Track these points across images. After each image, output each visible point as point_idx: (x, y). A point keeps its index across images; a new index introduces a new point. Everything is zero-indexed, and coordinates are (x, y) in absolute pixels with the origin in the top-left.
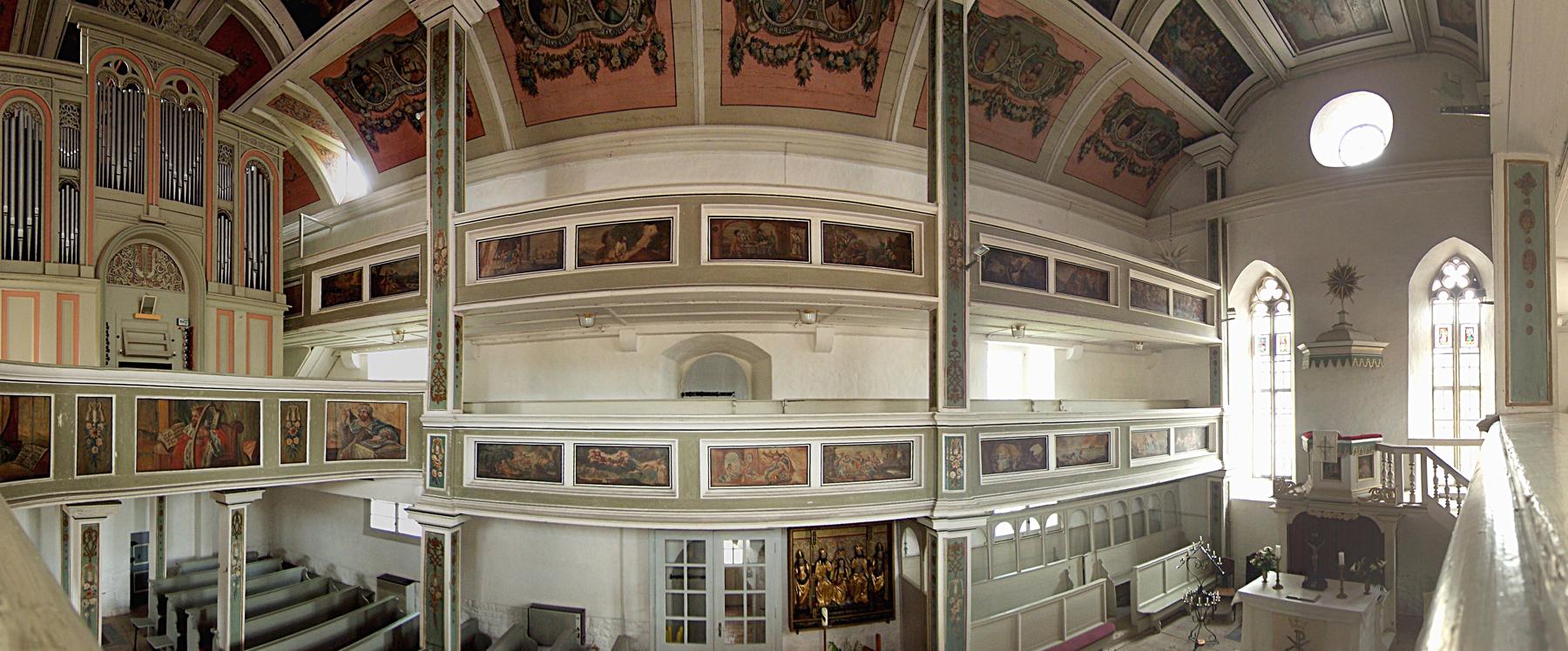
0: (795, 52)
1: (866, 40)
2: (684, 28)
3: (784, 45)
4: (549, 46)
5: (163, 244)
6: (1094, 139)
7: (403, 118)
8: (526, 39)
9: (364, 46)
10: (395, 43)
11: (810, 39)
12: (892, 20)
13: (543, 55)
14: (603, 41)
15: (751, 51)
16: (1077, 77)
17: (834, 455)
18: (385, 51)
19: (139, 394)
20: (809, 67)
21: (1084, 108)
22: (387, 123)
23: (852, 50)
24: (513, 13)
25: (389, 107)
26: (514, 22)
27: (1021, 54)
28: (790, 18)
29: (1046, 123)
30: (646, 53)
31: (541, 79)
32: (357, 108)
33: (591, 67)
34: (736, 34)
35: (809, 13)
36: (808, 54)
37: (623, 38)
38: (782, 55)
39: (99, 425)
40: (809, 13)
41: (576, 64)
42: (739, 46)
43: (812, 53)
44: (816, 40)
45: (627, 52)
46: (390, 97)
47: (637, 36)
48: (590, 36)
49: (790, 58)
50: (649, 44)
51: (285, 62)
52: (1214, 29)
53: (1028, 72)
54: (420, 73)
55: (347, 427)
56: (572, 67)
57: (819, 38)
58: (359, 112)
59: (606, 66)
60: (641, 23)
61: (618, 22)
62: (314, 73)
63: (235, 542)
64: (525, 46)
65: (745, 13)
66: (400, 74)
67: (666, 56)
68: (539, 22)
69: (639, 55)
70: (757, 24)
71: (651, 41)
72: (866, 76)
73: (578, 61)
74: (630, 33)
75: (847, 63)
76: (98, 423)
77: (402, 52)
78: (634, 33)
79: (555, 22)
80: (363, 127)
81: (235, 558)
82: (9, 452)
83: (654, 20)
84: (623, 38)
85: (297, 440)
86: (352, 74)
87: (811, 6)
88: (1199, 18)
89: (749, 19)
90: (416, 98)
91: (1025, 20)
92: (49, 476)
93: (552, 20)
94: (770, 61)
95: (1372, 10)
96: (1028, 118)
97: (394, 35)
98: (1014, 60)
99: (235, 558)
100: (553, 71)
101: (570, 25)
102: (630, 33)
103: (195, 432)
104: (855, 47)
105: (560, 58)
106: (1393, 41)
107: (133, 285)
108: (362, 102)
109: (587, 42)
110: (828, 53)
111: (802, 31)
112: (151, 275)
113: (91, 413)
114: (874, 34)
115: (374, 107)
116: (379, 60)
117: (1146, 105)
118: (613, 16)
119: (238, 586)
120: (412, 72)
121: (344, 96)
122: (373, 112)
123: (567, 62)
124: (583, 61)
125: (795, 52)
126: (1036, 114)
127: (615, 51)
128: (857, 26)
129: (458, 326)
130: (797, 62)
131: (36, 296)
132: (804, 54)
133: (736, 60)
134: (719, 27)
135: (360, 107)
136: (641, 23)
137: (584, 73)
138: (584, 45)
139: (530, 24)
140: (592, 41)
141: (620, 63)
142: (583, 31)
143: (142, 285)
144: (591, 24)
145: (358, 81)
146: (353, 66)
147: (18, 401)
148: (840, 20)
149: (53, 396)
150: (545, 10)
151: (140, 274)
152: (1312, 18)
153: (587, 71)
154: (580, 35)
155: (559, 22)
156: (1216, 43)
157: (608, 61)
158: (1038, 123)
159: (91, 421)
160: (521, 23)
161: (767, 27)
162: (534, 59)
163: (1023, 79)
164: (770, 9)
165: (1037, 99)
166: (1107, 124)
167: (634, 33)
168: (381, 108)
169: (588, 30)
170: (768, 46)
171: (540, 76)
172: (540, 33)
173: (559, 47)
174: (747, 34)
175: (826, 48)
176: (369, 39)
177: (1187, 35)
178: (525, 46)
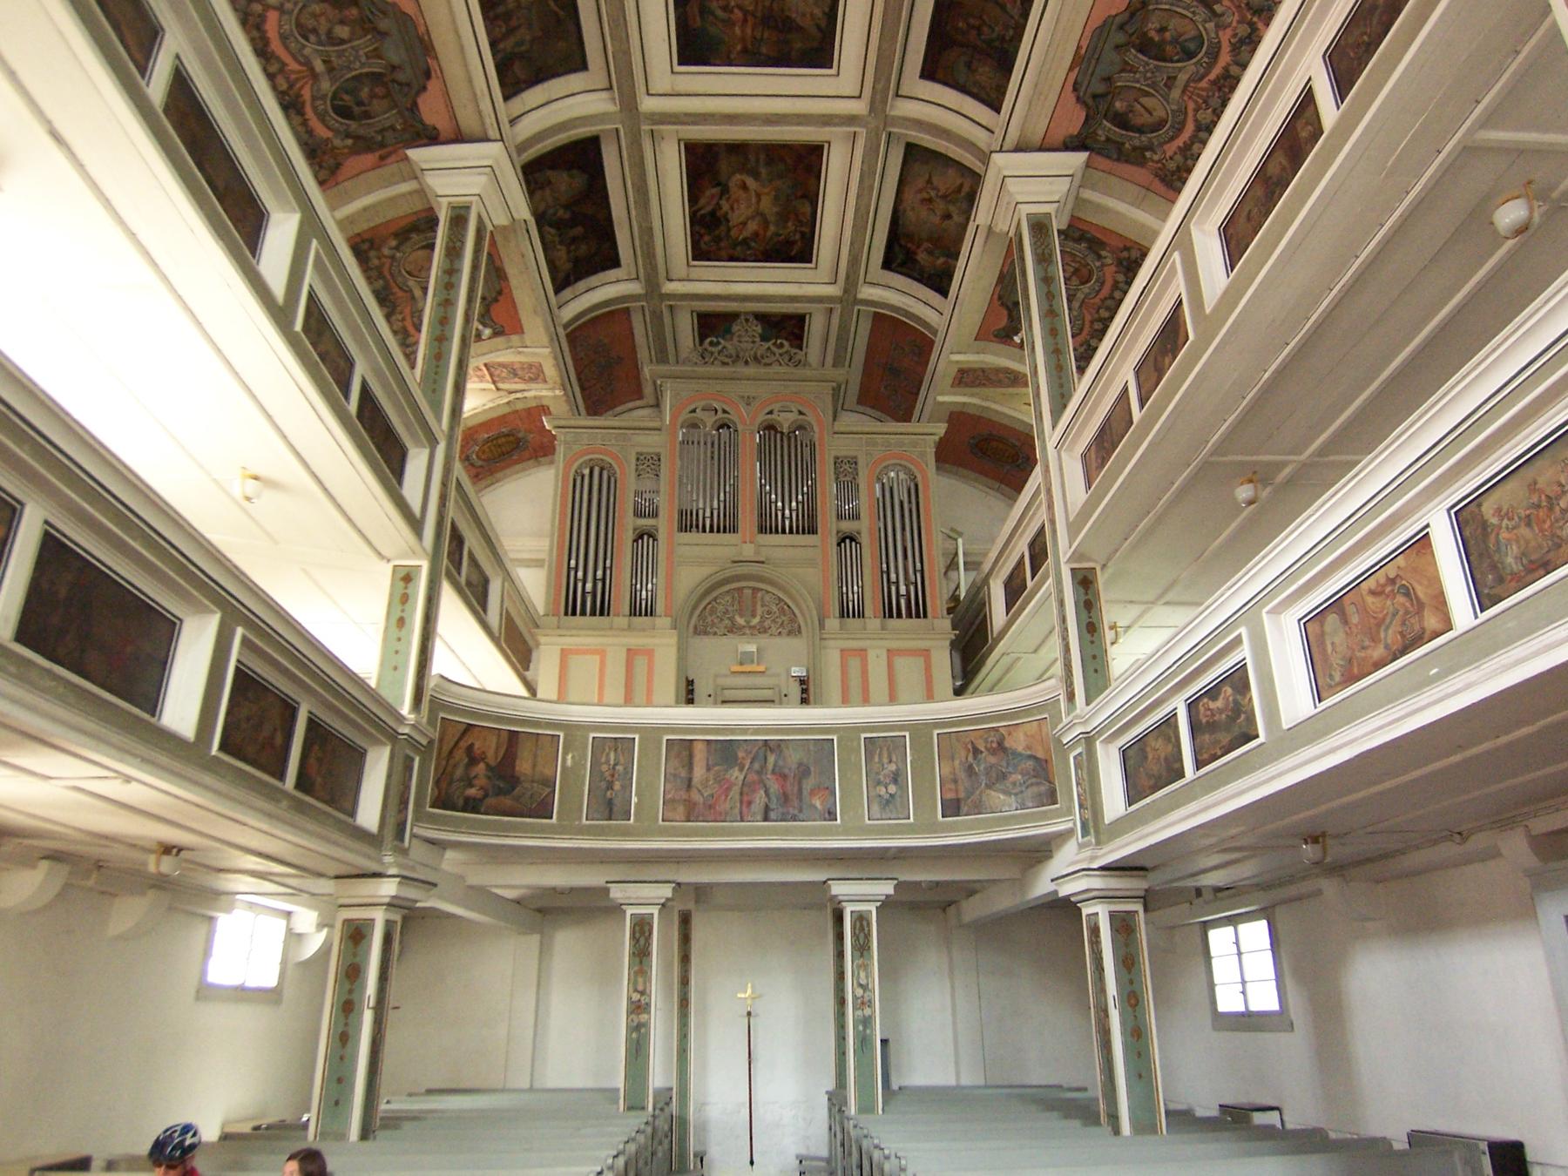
4: (1172, 139)
5: (739, 581)
8: (1148, 154)
13: (1175, 153)
14: (1212, 76)
17: (1484, 525)
19: (668, 734)
37: (1226, 48)
39: (617, 768)
48: (1195, 88)
50: (1255, 19)
55: (971, 767)
60: (1222, 15)
63: (861, 961)
64: (1153, 161)
68: (1140, 130)
71: (1253, 14)
76: (615, 765)
78: (1229, 32)
79: (1151, 114)
81: (861, 985)
82: (502, 785)
84: (1226, 48)
85: (892, 789)
92: (551, 818)
93: (1146, 115)
99: (861, 985)
101: (1168, 103)
102: (1225, 37)
103: (742, 777)
107: (730, 635)
109: (1199, 95)
112: (755, 621)
113: (608, 755)
118: (1192, 46)
119: (868, 1031)
131: (601, 653)
136: (1222, 15)
139: (1133, 140)
140: (1202, 89)
142: (1184, 92)
143: (744, 634)
144: (1182, 78)
147: (518, 738)
149: (562, 735)
150: (1130, 115)
151: (741, 621)
154: (1186, 98)
155: (1155, 110)
159: (607, 762)
160: (1127, 145)
162: (1172, 166)
167: (1229, 32)
172: (1150, 139)
178: (1153, 161)
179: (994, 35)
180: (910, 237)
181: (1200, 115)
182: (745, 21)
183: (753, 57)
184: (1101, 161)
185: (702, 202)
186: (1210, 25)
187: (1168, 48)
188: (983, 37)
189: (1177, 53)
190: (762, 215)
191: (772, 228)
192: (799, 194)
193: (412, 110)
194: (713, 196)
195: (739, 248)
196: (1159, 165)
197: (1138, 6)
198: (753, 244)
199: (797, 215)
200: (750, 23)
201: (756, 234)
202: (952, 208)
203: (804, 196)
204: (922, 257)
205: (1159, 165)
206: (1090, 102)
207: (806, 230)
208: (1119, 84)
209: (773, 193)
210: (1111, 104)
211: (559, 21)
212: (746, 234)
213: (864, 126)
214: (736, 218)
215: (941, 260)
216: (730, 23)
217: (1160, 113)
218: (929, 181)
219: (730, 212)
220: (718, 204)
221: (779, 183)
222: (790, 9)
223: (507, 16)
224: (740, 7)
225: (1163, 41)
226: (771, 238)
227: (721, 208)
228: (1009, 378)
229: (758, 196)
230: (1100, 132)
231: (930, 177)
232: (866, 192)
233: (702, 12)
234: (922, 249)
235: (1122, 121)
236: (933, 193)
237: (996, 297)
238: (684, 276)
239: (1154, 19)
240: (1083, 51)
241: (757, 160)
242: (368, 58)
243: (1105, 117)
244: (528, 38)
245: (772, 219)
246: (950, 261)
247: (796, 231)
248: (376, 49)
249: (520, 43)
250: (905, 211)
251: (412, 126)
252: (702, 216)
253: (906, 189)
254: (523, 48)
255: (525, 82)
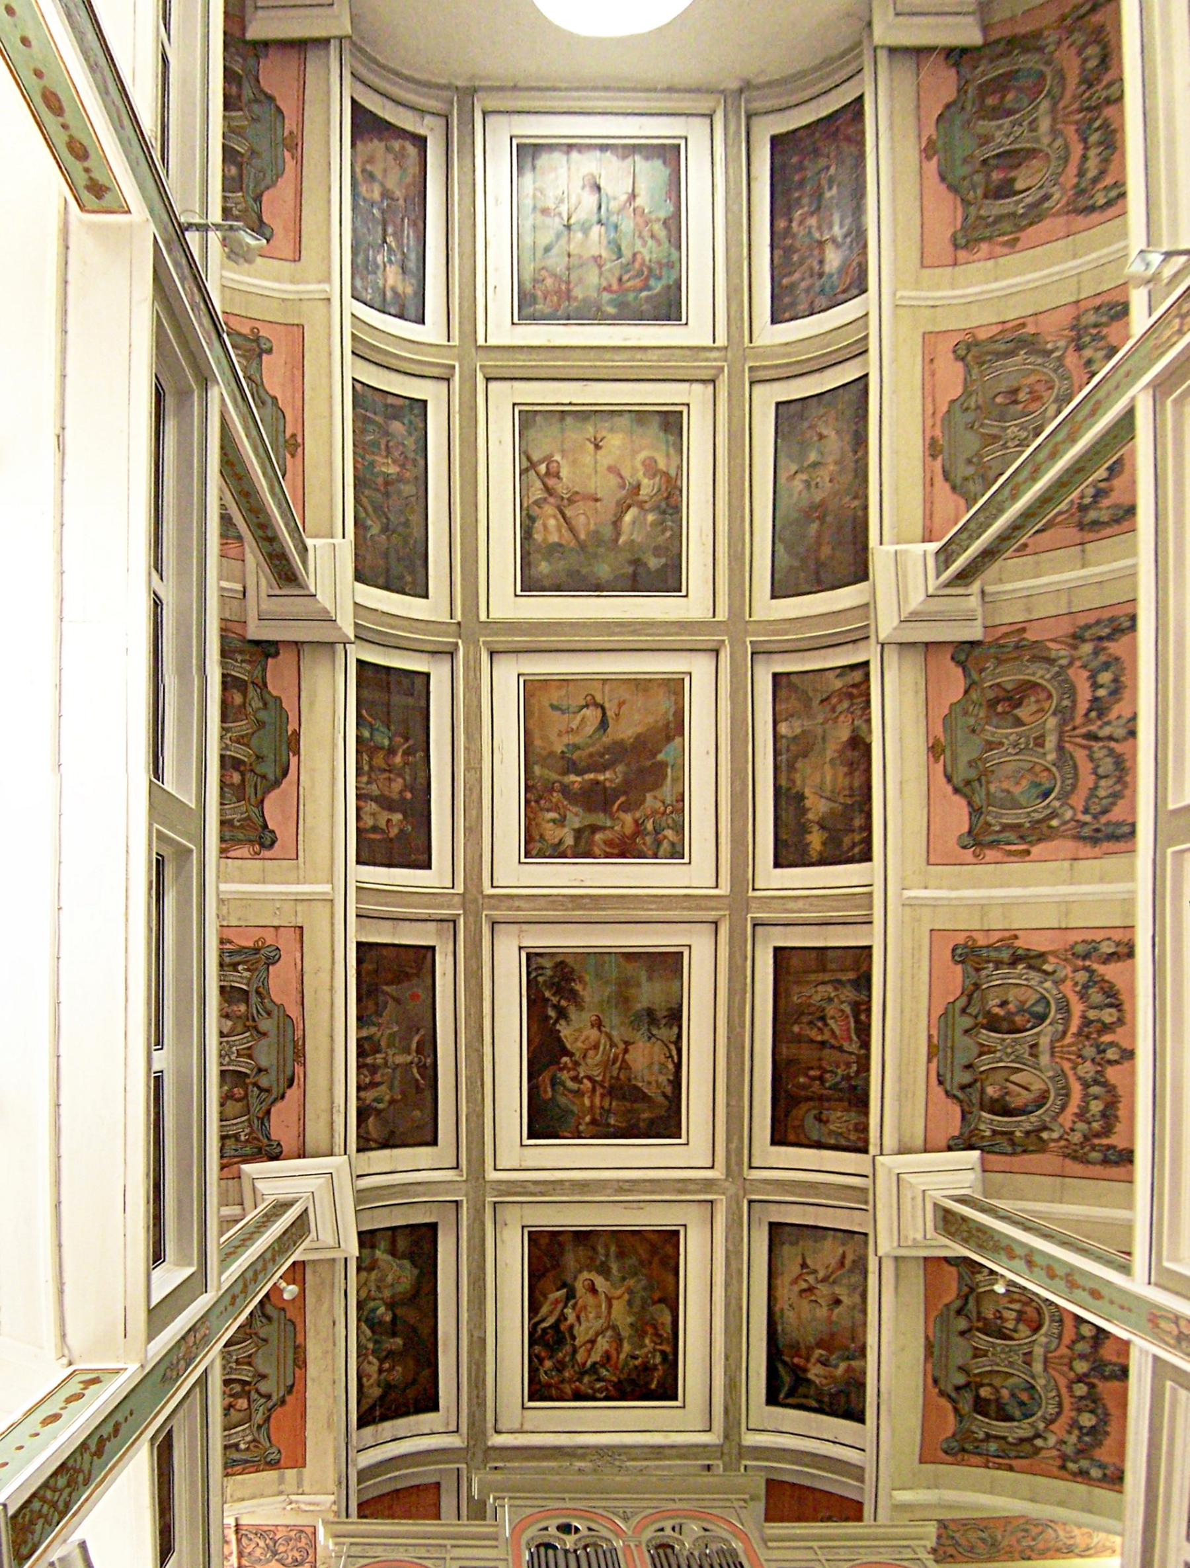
0: (1101, 748)
1: (1062, 653)
2: (1067, 914)
3: (1091, 765)
4: (1063, 1108)
6: (1082, 202)
7: (1092, 1386)
8: (1045, 1135)
9: (932, 1353)
10: (959, 1312)
11: (1077, 732)
12: (1024, 630)
13: (1074, 1122)
14: (1073, 1029)
15: (1105, 811)
16: (982, 335)
18: (962, 1333)
20: (1123, 721)
21: (1045, 272)
22: (1087, 1420)
23: (1084, 667)
24: (999, 1139)
25: (1059, 1396)
26: (1013, 1143)
27: (995, 438)
28: (1047, 769)
29: (1097, 309)
30: (1100, 969)
31: (1113, 1136)
32: (1027, 1447)
33: (1111, 1054)
34: (1078, 838)
35: (1036, 745)
36: (1101, 727)
37: (1074, 999)
38: (1107, 766)
40: (1036, 745)
41: (1103, 1076)
42: (1097, 830)
43: (1099, 723)
44: (1079, 720)
45: (1096, 997)
46: (1042, 1382)
47: (1073, 979)
48: (1062, 1047)
49: (1111, 752)
51: (869, 1475)
52: (778, 252)
53: (1020, 407)
54: (1028, 1309)
56: (1105, 1084)
57: (1072, 719)
58: (1038, 1450)
59: (1114, 1032)
61: (1048, 1003)
62: (917, 1450)
65: (1045, 829)
66: (1012, 1339)
67: (1109, 939)
68: (1022, 1111)
69: (1103, 980)
70: (1060, 811)
72: (1123, 631)
73: (1097, 1072)
74: (1067, 989)
75: (1106, 666)
77: (979, 1313)
78: (1069, 983)
80: (1070, 1465)
83: (1054, 953)
84: (1074, 999)
86: (966, 1407)
87: (1027, 744)
88: (785, 281)
89: (1054, 823)
90: (1066, 1340)
91: (943, 467)
94: (1120, 780)
95: (534, 182)
96: (1102, 344)
97: (947, 1305)
98: (1013, 439)
100: (1104, 1115)
101: (1040, 1070)
102: (1067, 989)
104: (1078, 663)
105: (1086, 1098)
106: (515, 118)
108: (1022, 1430)
109: (1069, 1053)
110: (1095, 699)
111: (1067, 745)
114: (1050, 645)
115: (1043, 1418)
116: (970, 1353)
117: (949, 196)
118: (1039, 1009)
120: (1019, 1320)
121: (993, 1447)
122: (1052, 1427)
123: (1095, 1090)
124: (1099, 1064)
125: (1101, 748)
126: (1087, 339)
127: (1092, 1014)
128: (1042, 677)
129: (440, 1546)
130: (1116, 740)
132: (1101, 734)
133: (1119, 832)
134: (1066, 864)
135: (1029, 1440)
136: (1054, 972)
137: (1118, 1067)
138: (1073, 1057)
139: (1021, 1125)
140: (1069, 1045)
141: (1113, 1010)
142: (1052, 1054)
144: (1044, 1041)
145: (980, 1406)
146: (954, 1395)
148: (1037, 701)
150: (1007, 1098)
152: (633, 196)
153: (1117, 1062)
154: (1058, 1060)
156: (789, 227)
157: (1106, 1028)
158: (1104, 319)
160: (1018, 1134)
161: (1065, 796)
162: (1076, 1138)
163: (1038, 404)
164: (1038, 797)
165: (1059, 358)
166: (1036, 213)
167: (1069, 983)
168: (1052, 1410)
169: (1052, 1048)
170: (1096, 788)
171: (1108, 1137)
173: (1067, 1095)
174: (1077, 821)
175: (1087, 705)
176: (927, 1338)
177: (817, 268)
179: (838, 1078)
180: (795, 1348)
181: (1081, 1071)
182: (594, 1090)
183: (602, 1130)
184: (995, 1160)
185: (544, 1310)
186: (1048, 985)
187: (1018, 1019)
188: (827, 1085)
189: (1029, 1021)
190: (614, 1328)
191: (627, 1347)
192: (657, 1295)
193: (262, 1119)
194: (557, 1302)
195: (586, 1379)
196: (1063, 1143)
197: (972, 988)
198: (604, 1372)
199: (655, 1327)
200: (598, 1093)
201: (607, 1356)
202: (838, 1290)
203: (661, 1300)
204: (815, 1372)
205: (1063, 1143)
206: (959, 1094)
207: (667, 1348)
208: (982, 1069)
209: (626, 1297)
210: (983, 1091)
211: (417, 1086)
212: (596, 1357)
213: (723, 1194)
214: (582, 1333)
215: (843, 1366)
216: (579, 1093)
217: (1037, 1086)
218: (804, 1265)
219: (577, 1325)
220: (562, 1313)
221: (631, 1282)
222: (635, 1078)
223: (374, 1069)
224: (589, 1078)
225: (1010, 1013)
226: (626, 1363)
227: (566, 1319)
228: (983, 1540)
229: (609, 1301)
230: (982, 1127)
231: (804, 1258)
232: (734, 1281)
233: (553, 1085)
234: (813, 1360)
235: (1001, 1108)
236: (811, 1279)
237: (930, 1381)
238: (516, 1426)
239: (991, 996)
240: (935, 1041)
241: (607, 1255)
242: (239, 1055)
243: (982, 1109)
244: (387, 1098)
245: (626, 1333)
246: (853, 1363)
247: (655, 1350)
248: (249, 1048)
249: (378, 1100)
250: (782, 1310)
251: (258, 1139)
252: (544, 1330)
253: (779, 1282)
254: (381, 1106)
255: (375, 1141)
